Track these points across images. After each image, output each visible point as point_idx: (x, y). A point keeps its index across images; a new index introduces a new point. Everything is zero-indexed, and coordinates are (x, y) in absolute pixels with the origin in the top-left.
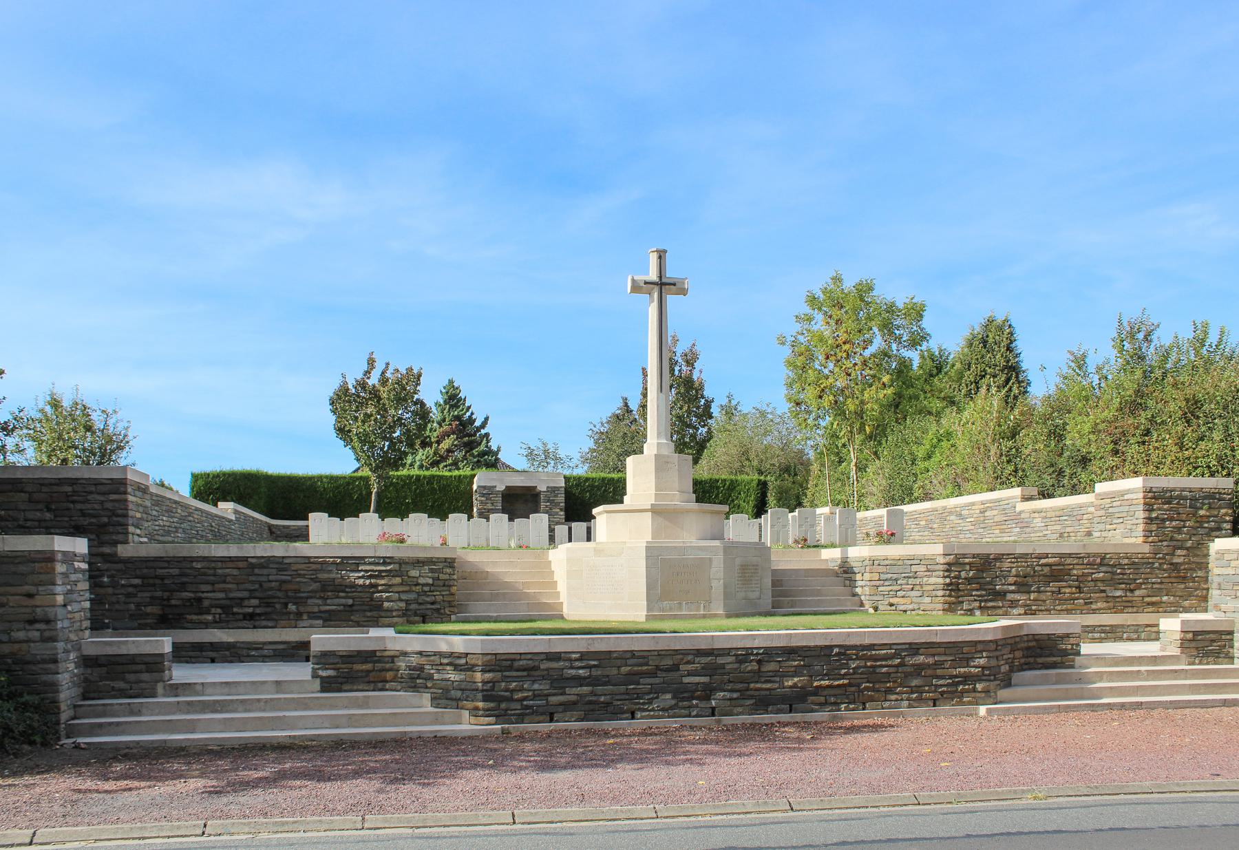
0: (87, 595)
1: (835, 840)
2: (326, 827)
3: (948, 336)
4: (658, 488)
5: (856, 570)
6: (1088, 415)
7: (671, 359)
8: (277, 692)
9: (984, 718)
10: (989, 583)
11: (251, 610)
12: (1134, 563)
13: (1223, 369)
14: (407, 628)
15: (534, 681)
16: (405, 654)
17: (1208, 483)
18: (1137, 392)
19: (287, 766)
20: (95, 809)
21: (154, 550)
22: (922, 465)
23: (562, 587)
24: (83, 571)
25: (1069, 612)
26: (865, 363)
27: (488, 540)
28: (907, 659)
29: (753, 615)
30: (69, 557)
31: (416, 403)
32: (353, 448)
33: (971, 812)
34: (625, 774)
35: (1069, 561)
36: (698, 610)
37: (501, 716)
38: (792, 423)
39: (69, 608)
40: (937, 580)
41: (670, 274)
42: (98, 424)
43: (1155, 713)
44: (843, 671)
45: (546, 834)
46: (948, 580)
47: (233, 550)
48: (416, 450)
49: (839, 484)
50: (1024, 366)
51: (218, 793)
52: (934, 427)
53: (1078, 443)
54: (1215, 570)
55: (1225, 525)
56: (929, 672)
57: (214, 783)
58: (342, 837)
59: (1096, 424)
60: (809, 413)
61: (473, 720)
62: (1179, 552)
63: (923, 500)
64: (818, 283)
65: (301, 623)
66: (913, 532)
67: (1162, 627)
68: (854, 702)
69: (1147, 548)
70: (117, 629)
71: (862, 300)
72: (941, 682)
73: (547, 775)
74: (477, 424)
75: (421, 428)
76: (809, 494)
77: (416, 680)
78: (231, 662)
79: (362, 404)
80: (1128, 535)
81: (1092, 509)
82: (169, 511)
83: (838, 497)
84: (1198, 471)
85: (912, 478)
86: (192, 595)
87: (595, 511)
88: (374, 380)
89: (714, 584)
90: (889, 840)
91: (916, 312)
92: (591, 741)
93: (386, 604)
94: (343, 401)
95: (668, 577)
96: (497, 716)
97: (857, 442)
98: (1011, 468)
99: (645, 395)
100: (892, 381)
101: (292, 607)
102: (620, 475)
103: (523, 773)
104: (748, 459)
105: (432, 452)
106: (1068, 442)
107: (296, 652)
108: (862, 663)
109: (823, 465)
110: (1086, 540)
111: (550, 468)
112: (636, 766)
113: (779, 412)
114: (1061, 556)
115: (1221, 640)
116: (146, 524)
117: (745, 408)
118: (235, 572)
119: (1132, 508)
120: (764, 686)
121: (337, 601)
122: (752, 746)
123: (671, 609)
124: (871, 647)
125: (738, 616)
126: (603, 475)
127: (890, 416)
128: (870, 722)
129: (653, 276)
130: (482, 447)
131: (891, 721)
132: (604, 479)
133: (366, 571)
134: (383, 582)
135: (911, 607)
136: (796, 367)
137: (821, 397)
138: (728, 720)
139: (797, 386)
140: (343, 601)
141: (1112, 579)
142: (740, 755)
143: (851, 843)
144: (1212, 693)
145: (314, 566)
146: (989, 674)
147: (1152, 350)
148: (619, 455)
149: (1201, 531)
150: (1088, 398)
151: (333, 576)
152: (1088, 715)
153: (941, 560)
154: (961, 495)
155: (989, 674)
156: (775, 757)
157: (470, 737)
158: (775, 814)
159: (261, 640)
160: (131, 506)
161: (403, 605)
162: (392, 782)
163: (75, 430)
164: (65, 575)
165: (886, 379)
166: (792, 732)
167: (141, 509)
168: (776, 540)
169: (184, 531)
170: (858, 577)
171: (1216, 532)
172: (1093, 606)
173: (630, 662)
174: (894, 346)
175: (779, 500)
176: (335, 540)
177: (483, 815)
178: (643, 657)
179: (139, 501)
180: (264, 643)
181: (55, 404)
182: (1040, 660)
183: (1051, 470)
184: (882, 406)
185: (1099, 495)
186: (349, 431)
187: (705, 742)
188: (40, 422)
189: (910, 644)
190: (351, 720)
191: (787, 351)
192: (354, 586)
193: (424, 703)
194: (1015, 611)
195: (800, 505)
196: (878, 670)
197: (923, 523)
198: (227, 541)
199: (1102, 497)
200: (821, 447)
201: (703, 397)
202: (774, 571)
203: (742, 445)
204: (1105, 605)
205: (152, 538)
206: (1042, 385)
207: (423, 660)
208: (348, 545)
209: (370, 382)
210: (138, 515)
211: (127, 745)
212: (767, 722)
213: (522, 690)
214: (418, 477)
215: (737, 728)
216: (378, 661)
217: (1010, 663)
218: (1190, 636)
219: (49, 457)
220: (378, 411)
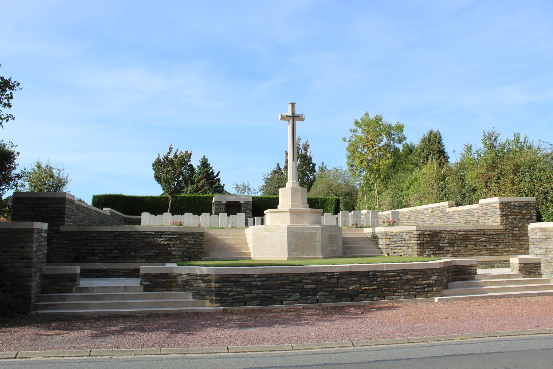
0: (46, 248)
1: (373, 360)
2: (144, 353)
3: (414, 137)
4: (293, 202)
5: (379, 237)
6: (474, 171)
7: (297, 147)
8: (125, 292)
9: (437, 303)
10: (437, 243)
11: (115, 255)
12: (497, 234)
13: (527, 152)
14: (182, 263)
15: (238, 287)
16: (181, 275)
17: (525, 199)
18: (493, 161)
19: (128, 325)
20: (43, 343)
21: (75, 228)
22: (406, 192)
23: (250, 245)
24: (45, 237)
25: (471, 255)
26: (380, 149)
27: (218, 224)
28: (403, 277)
29: (335, 257)
30: (40, 231)
31: (189, 166)
32: (162, 185)
33: (433, 346)
34: (278, 330)
35: (470, 233)
36: (310, 255)
37: (223, 303)
38: (350, 174)
39: (38, 253)
40: (414, 242)
41: (297, 112)
42: (56, 175)
43: (510, 299)
44: (375, 282)
45: (243, 357)
46: (419, 242)
47: (108, 229)
48: (189, 185)
49: (371, 200)
50: (446, 150)
51: (97, 337)
52: (410, 176)
53: (471, 182)
54: (531, 236)
55: (533, 217)
56: (412, 283)
57: (95, 332)
58: (151, 358)
59: (478, 175)
60: (357, 170)
61: (210, 305)
62: (516, 229)
63: (407, 207)
64: (359, 116)
65: (136, 261)
66: (403, 221)
67: (511, 262)
68: (380, 297)
69: (502, 227)
70: (58, 263)
71: (377, 123)
72: (418, 287)
73: (243, 330)
74: (215, 174)
75: (191, 176)
76: (358, 204)
77: (186, 286)
78: (105, 278)
79: (166, 166)
80: (494, 222)
81: (478, 211)
82: (83, 212)
83: (370, 206)
84: (521, 194)
85: (401, 198)
86: (90, 248)
87: (265, 212)
88: (171, 156)
89: (317, 244)
90: (397, 359)
91: (400, 128)
92: (263, 315)
93: (173, 253)
94: (159, 165)
95: (297, 241)
96: (221, 303)
97: (378, 182)
98: (443, 193)
99: (287, 162)
100: (391, 156)
101: (133, 254)
102: (276, 196)
103: (232, 329)
104: (331, 189)
105: (195, 186)
106: (467, 182)
107: (134, 274)
108: (383, 279)
109: (363, 192)
110: (477, 224)
111: (246, 193)
112: (283, 326)
113: (344, 169)
114: (467, 231)
115: (535, 267)
116: (72, 217)
117: (330, 168)
118: (109, 238)
119: (495, 210)
120: (340, 289)
121: (152, 251)
122: (335, 317)
123: (298, 255)
124: (387, 271)
125: (328, 258)
126: (269, 196)
127: (391, 171)
128: (387, 305)
129: (290, 113)
130: (217, 184)
131: (397, 305)
132: (269, 198)
133: (165, 238)
134: (172, 243)
135: (403, 254)
136: (351, 151)
137: (362, 163)
138: (324, 305)
139: (351, 159)
140: (155, 251)
141: (489, 241)
142: (329, 321)
143: (380, 361)
144: (534, 290)
145: (143, 236)
146: (438, 283)
147: (498, 144)
148: (275, 188)
149: (524, 220)
150: (473, 163)
151: (151, 240)
152: (482, 301)
153: (416, 233)
154: (423, 205)
155: (438, 283)
156: (346, 322)
157: (209, 313)
158: (346, 348)
159: (119, 268)
160: (67, 209)
161: (181, 253)
162: (174, 333)
163: (46, 177)
164: (37, 239)
165: (389, 156)
166: (353, 310)
167: (71, 211)
168: (344, 224)
169: (88, 221)
170: (380, 240)
171: (530, 220)
172: (482, 253)
173: (280, 278)
174: (392, 142)
175: (345, 207)
176: (152, 224)
177: (214, 348)
178: (286, 276)
179: (70, 207)
180: (120, 270)
181: (39, 166)
182: (460, 277)
183: (460, 194)
184: (387, 167)
185: (481, 204)
186: (160, 178)
187: (314, 315)
188: (32, 174)
189: (404, 270)
190: (156, 305)
191: (347, 144)
192: (160, 244)
193: (189, 297)
194: (448, 255)
195: (354, 209)
196: (390, 282)
197: (407, 217)
198: (106, 225)
199: (482, 205)
200: (362, 184)
201: (311, 163)
202: (344, 238)
203: (328, 183)
204: (486, 252)
205: (75, 223)
206: (454, 159)
207: (189, 278)
208: (158, 227)
209: (170, 157)
210: (70, 213)
211: (59, 314)
212: (341, 305)
213: (232, 291)
214: (189, 197)
215: (328, 309)
216: (170, 278)
217: (447, 278)
218: (523, 265)
219: (35, 188)
220: (171, 169)
